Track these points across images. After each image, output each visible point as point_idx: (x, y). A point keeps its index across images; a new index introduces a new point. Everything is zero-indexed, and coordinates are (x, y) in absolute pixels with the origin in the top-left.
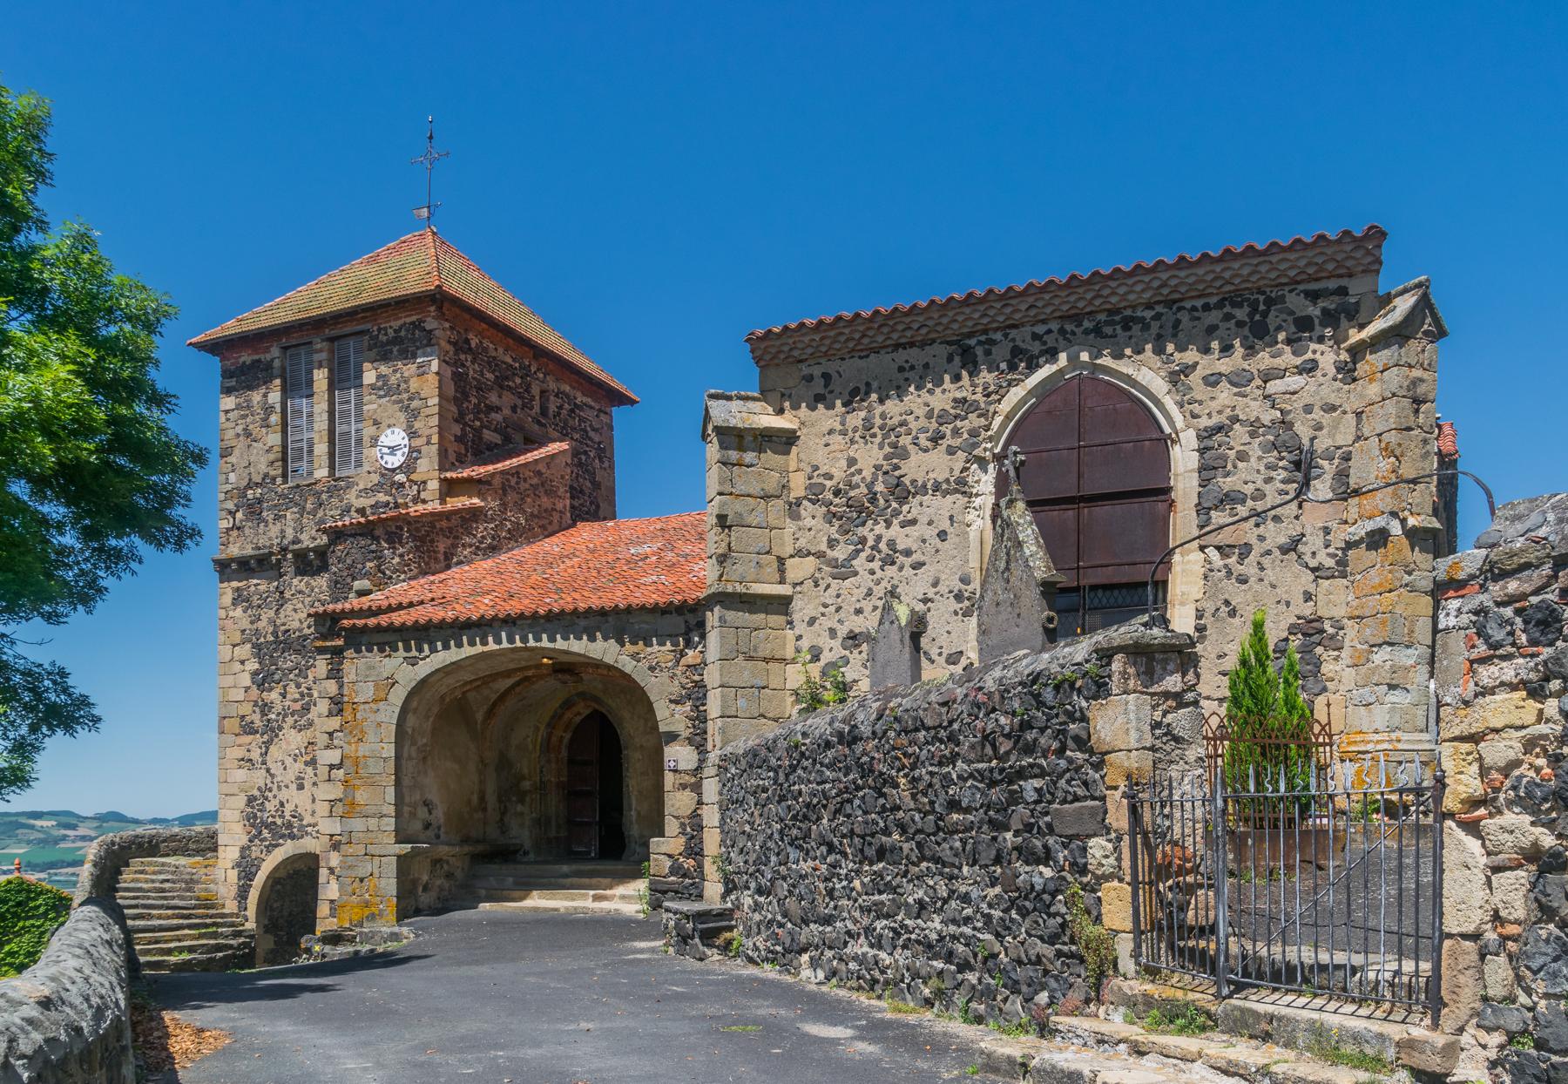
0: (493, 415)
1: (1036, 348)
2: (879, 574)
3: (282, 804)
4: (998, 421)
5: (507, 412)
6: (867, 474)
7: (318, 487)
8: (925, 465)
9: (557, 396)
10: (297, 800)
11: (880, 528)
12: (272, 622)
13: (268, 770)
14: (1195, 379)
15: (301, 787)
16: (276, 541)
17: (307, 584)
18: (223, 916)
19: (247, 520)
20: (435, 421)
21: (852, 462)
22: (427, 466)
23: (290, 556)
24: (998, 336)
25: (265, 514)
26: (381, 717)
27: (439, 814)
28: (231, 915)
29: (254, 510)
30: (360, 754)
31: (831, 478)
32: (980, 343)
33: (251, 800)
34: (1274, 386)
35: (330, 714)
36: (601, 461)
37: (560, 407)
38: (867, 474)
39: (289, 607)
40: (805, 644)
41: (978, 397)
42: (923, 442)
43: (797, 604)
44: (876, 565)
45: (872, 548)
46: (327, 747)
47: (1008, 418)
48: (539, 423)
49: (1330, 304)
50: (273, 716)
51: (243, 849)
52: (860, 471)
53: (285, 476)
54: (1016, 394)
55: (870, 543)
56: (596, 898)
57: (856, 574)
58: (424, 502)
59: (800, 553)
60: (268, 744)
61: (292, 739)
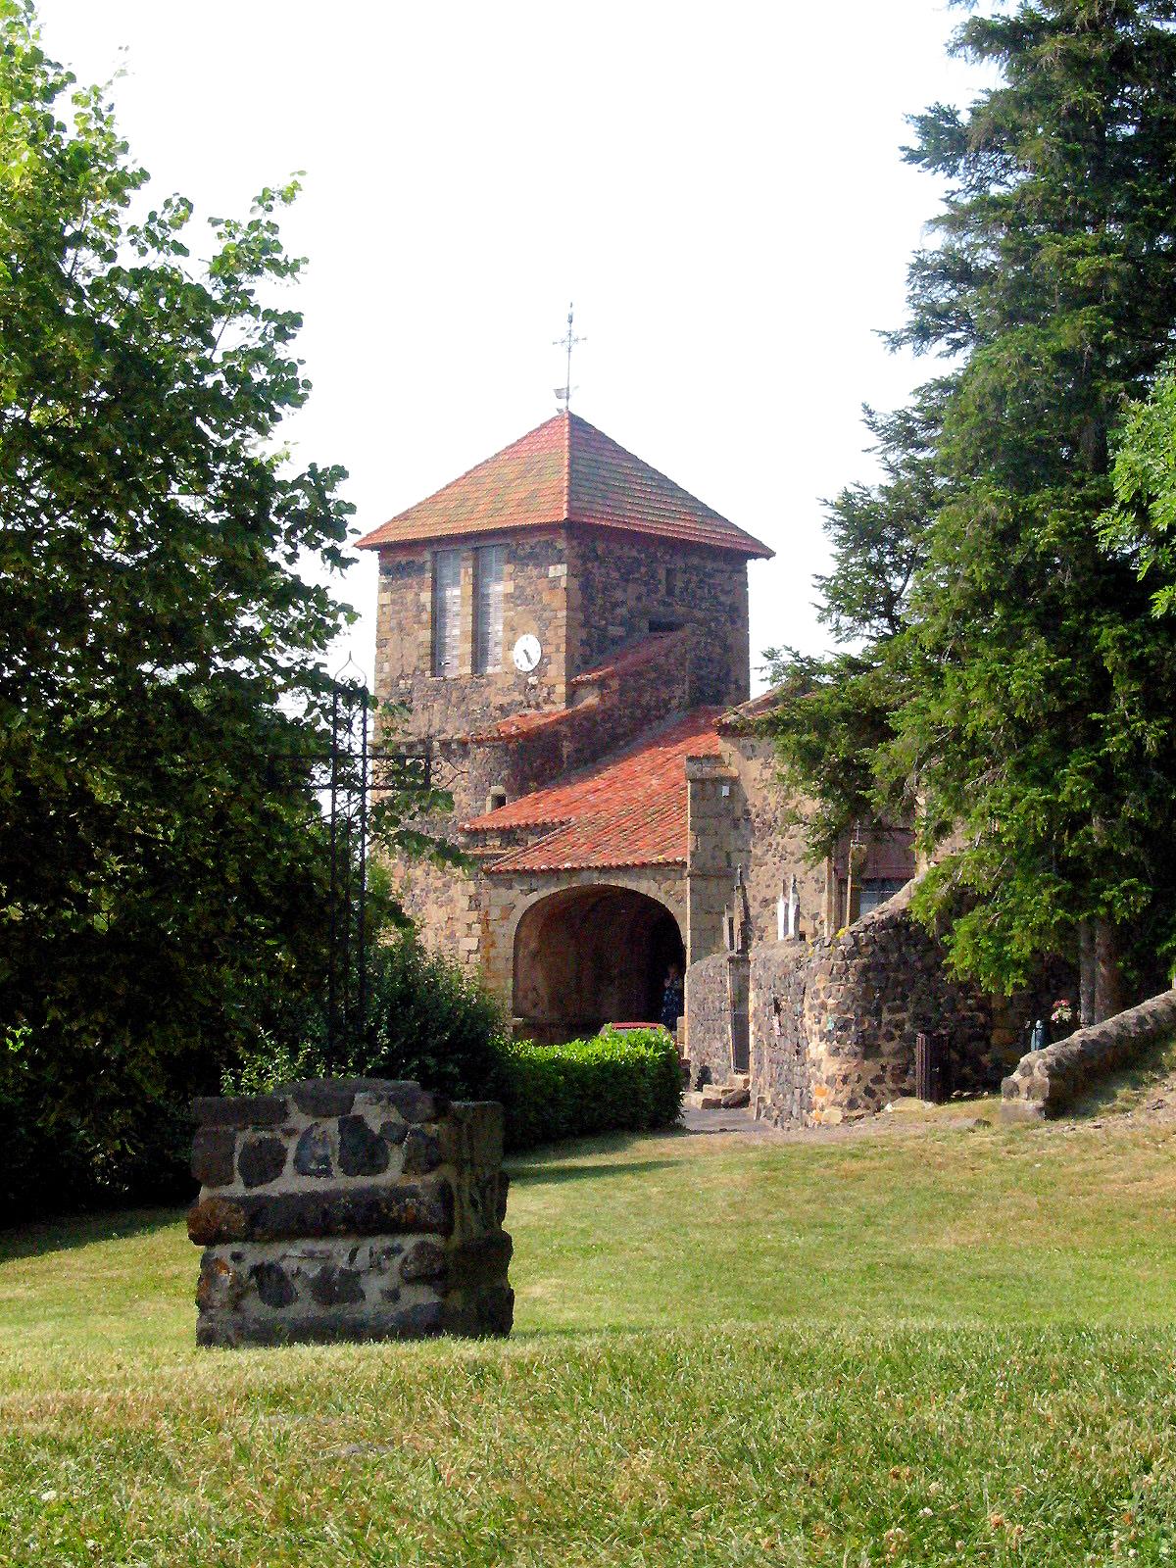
5: (632, 603)
16: (424, 730)
20: (563, 631)
22: (557, 672)
27: (544, 991)
37: (689, 582)
38: (773, 805)
48: (664, 603)
50: (417, 892)
53: (432, 669)
58: (553, 703)
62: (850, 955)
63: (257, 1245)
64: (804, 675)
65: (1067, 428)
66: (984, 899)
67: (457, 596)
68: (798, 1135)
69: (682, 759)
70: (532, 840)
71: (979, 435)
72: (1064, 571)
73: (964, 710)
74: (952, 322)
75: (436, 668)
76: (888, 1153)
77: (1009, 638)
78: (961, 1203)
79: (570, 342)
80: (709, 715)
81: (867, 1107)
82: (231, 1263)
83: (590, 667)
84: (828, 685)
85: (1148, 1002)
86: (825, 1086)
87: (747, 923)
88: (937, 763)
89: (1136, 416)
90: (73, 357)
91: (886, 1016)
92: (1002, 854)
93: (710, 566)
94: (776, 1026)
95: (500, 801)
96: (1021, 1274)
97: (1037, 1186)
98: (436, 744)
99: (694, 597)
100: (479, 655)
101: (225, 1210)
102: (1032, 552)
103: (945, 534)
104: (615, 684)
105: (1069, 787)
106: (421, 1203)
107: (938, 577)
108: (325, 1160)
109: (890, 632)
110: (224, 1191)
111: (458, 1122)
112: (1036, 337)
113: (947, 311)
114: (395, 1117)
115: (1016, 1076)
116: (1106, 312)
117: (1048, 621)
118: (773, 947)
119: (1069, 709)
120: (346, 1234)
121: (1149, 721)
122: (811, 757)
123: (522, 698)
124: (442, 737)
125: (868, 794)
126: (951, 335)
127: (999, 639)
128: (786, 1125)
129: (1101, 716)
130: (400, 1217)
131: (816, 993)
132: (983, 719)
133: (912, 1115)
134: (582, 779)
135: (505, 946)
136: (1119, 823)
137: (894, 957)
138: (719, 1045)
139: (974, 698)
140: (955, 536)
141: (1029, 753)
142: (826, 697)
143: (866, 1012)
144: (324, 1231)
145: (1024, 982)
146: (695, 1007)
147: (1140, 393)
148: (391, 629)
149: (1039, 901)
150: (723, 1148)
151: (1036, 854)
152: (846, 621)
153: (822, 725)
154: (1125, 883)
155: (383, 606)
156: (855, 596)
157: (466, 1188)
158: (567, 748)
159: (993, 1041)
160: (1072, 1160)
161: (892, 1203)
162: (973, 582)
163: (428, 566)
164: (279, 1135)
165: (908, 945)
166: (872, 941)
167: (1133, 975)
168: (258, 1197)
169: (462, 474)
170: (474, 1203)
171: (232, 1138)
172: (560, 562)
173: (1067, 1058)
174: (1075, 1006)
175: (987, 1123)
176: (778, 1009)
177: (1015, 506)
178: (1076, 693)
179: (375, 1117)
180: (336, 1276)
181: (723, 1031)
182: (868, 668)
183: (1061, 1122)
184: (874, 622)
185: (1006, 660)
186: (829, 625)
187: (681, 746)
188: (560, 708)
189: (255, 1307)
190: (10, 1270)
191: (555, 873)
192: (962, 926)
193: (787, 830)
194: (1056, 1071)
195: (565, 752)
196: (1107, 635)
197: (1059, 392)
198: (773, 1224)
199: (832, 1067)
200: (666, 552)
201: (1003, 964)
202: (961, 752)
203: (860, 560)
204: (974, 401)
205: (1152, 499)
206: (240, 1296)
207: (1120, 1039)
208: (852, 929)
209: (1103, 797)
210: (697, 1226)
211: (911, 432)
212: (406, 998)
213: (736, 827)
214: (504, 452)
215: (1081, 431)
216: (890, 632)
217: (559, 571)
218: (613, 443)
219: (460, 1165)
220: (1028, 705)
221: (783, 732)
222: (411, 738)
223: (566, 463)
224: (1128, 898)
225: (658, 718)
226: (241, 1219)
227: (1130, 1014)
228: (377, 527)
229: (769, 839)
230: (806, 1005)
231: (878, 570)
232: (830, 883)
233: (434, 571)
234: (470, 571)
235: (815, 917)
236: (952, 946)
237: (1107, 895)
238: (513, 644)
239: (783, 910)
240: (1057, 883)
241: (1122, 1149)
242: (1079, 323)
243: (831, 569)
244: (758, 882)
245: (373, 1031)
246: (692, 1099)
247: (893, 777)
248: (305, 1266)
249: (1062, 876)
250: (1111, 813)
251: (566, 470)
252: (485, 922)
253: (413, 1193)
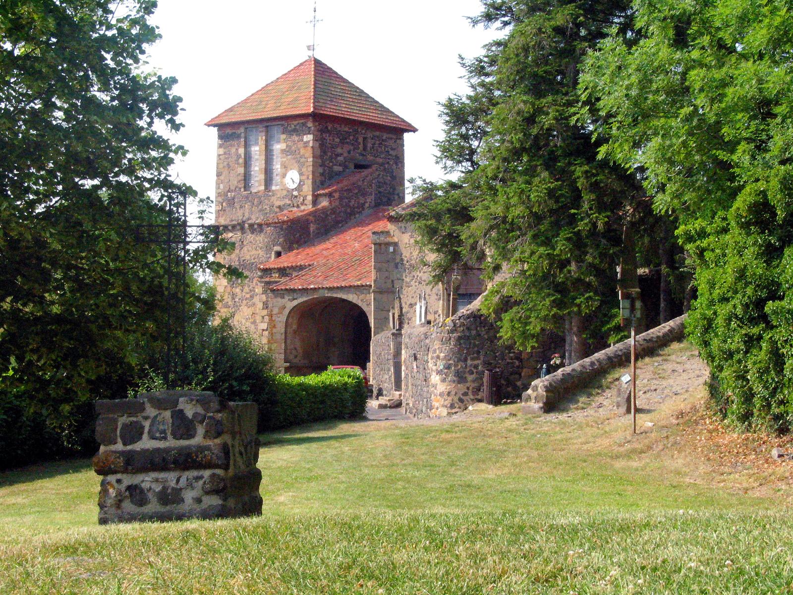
0: (339, 158)
5: (346, 154)
7: (259, 194)
16: (240, 218)
17: (254, 239)
19: (228, 207)
20: (311, 169)
21: (411, 253)
22: (308, 189)
25: (236, 204)
27: (300, 350)
29: (231, 202)
35: (263, 309)
39: (245, 249)
48: (363, 155)
50: (237, 300)
53: (245, 187)
58: (306, 205)
62: (452, 331)
63: (129, 475)
64: (429, 190)
65: (560, 66)
66: (517, 303)
67: (257, 150)
68: (426, 422)
69: (370, 233)
70: (294, 274)
71: (516, 69)
72: (558, 138)
73: (507, 208)
74: (503, 12)
75: (247, 187)
76: (464, 430)
77: (531, 172)
78: (499, 455)
79: (314, 21)
80: (385, 211)
81: (460, 408)
82: (116, 485)
83: (325, 186)
84: (440, 196)
85: (596, 354)
86: (439, 397)
87: (401, 316)
88: (494, 234)
89: (591, 58)
90: (33, 19)
91: (469, 362)
92: (526, 281)
93: (385, 136)
94: (415, 367)
95: (278, 254)
96: (526, 490)
97: (538, 447)
98: (246, 225)
99: (377, 150)
100: (268, 180)
101: (113, 457)
102: (542, 128)
103: (498, 119)
104: (337, 195)
105: (559, 247)
106: (213, 454)
107: (495, 141)
108: (164, 432)
109: (471, 169)
110: (113, 448)
111: (233, 412)
112: (544, 20)
113: (501, 7)
114: (200, 410)
115: (530, 391)
116: (579, 7)
117: (550, 163)
118: (414, 327)
119: (562, 207)
120: (174, 470)
121: (600, 213)
122: (432, 232)
123: (290, 202)
124: (250, 222)
125: (459, 249)
126: (503, 19)
127: (525, 173)
128: (419, 417)
129: (576, 211)
130: (202, 460)
131: (435, 351)
132: (517, 212)
133: (482, 412)
134: (320, 243)
135: (281, 328)
136: (584, 265)
137: (474, 332)
138: (387, 377)
139: (513, 201)
140: (504, 119)
141: (539, 230)
142: (440, 202)
143: (459, 360)
144: (164, 468)
145: (536, 345)
146: (376, 358)
147: (593, 46)
148: (224, 167)
149: (544, 305)
150: (385, 429)
151: (543, 281)
152: (449, 163)
153: (438, 216)
154: (587, 295)
156: (455, 151)
157: (237, 447)
158: (312, 228)
159: (523, 374)
160: (556, 433)
161: (465, 455)
162: (512, 143)
163: (243, 135)
164: (140, 419)
165: (481, 327)
166: (463, 325)
167: (590, 341)
168: (130, 451)
169: (260, 88)
170: (241, 454)
171: (115, 421)
172: (309, 133)
173: (555, 382)
174: (563, 357)
175: (515, 415)
176: (416, 359)
177: (533, 104)
178: (563, 199)
179: (190, 411)
180: (169, 491)
181: (389, 370)
182: (461, 187)
183: (552, 414)
184: (463, 164)
185: (529, 183)
186: (441, 165)
187: (370, 227)
188: (309, 207)
189: (128, 506)
190: (16, 490)
191: (305, 291)
192: (506, 317)
193: (422, 269)
194: (549, 389)
195: (311, 229)
196: (579, 170)
197: (556, 47)
198: (405, 465)
199: (442, 388)
200: (363, 129)
201: (525, 335)
202: (506, 229)
203: (456, 132)
204: (513, 52)
205: (598, 99)
206: (120, 501)
207: (581, 373)
208: (453, 318)
209: (577, 253)
210: (366, 466)
211: (483, 68)
212: (222, 353)
213: (397, 267)
214: (281, 78)
215: (566, 67)
216: (471, 169)
217: (309, 138)
218: (336, 73)
219: (233, 435)
220: (539, 206)
221: (418, 220)
222: (234, 222)
223: (313, 83)
224: (588, 302)
225: (358, 213)
226: (121, 461)
227: (587, 360)
228: (217, 115)
229: (414, 273)
230: (430, 356)
231: (465, 137)
232: (443, 296)
233: (246, 138)
234: (264, 138)
235: (436, 313)
236: (502, 327)
237: (578, 301)
238: (285, 175)
239: (420, 308)
240: (553, 295)
241: (580, 427)
242: (566, 12)
243: (442, 137)
244: (409, 294)
245: (205, 368)
246: (373, 404)
247: (471, 241)
248: (154, 486)
249: (556, 291)
250: (580, 260)
251: (313, 87)
252: (271, 316)
253: (208, 448)
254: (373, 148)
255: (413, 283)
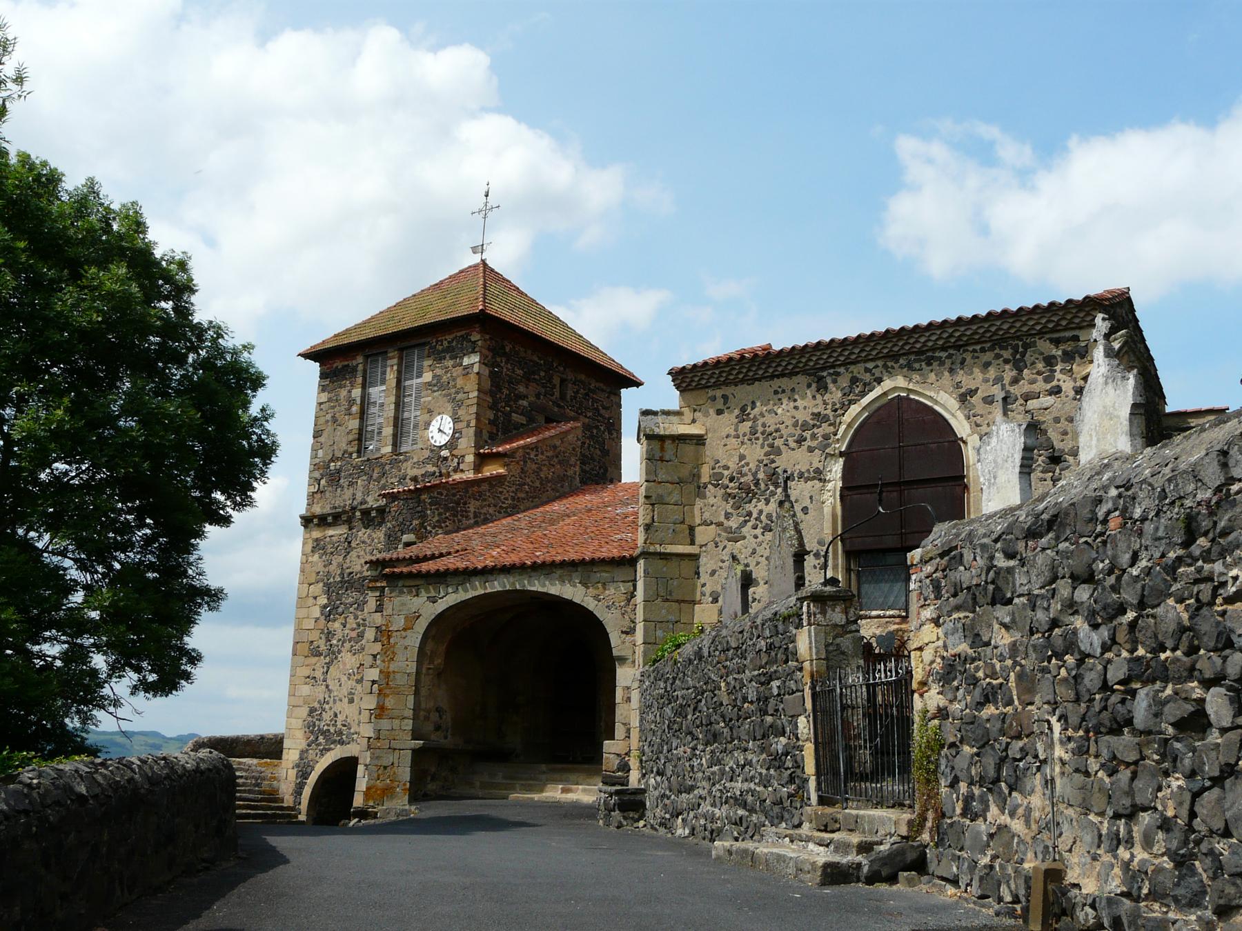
0: (521, 402)
1: (867, 377)
2: (761, 538)
3: (336, 715)
4: (843, 427)
5: (532, 399)
6: (752, 466)
7: (383, 460)
8: (795, 459)
9: (574, 383)
10: (347, 712)
11: (761, 505)
12: (341, 566)
13: (327, 686)
14: (976, 400)
15: (351, 701)
17: (370, 536)
18: (282, 808)
19: (329, 485)
20: (474, 409)
21: (742, 457)
22: (466, 445)
23: (358, 514)
24: (842, 370)
26: (407, 642)
27: (448, 717)
28: (288, 808)
30: (391, 670)
31: (728, 468)
32: (830, 374)
33: (312, 710)
34: (1032, 404)
35: (376, 640)
36: (610, 433)
37: (577, 392)
39: (354, 554)
40: (707, 590)
41: (829, 412)
42: (793, 445)
43: (703, 560)
44: (759, 531)
45: (756, 519)
46: (371, 667)
47: (849, 426)
48: (559, 406)
49: (1068, 347)
50: (334, 642)
51: (302, 752)
52: (748, 464)
53: (359, 452)
54: (854, 409)
55: (755, 515)
56: (564, 791)
57: (744, 538)
58: (462, 471)
59: (705, 523)
60: (329, 665)
61: (348, 660)
123: (435, 469)
155: (321, 404)
163: (360, 367)
217: (473, 359)
234: (395, 368)
254: (575, 398)
255: (746, 530)
